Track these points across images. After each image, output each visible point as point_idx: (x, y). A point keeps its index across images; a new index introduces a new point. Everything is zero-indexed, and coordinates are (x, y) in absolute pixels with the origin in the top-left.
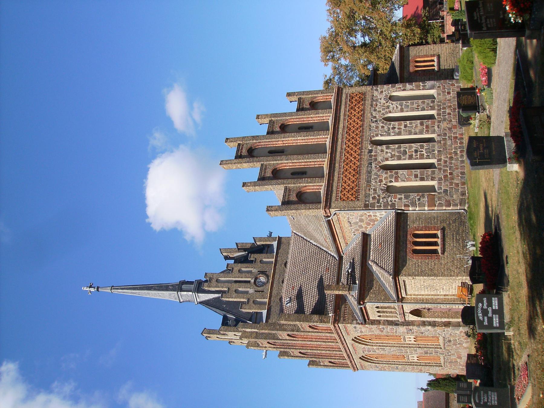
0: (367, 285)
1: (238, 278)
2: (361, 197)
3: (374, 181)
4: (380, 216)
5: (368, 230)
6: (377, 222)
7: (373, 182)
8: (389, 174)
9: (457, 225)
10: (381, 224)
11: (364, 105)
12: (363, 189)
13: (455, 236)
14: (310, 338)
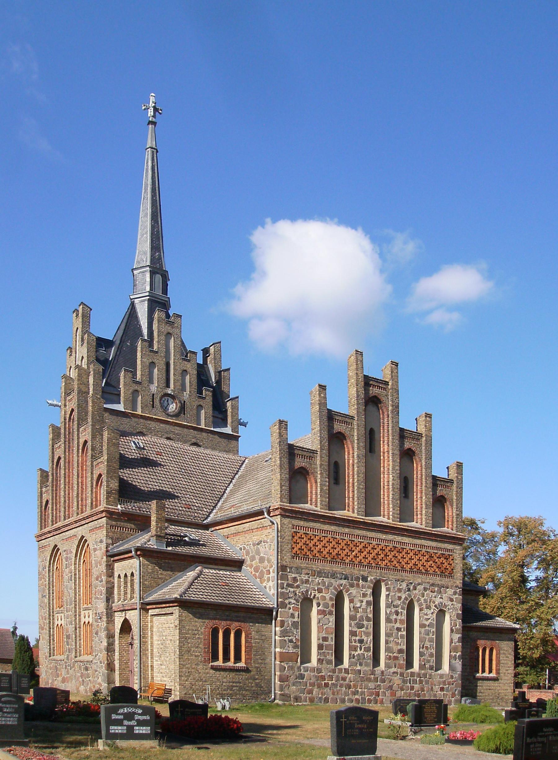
0: (165, 562)
1: (174, 369)
2: (298, 562)
3: (320, 581)
4: (268, 586)
5: (248, 568)
6: (259, 582)
9: (254, 688)
12: (310, 566)
13: (238, 684)
14: (82, 474)
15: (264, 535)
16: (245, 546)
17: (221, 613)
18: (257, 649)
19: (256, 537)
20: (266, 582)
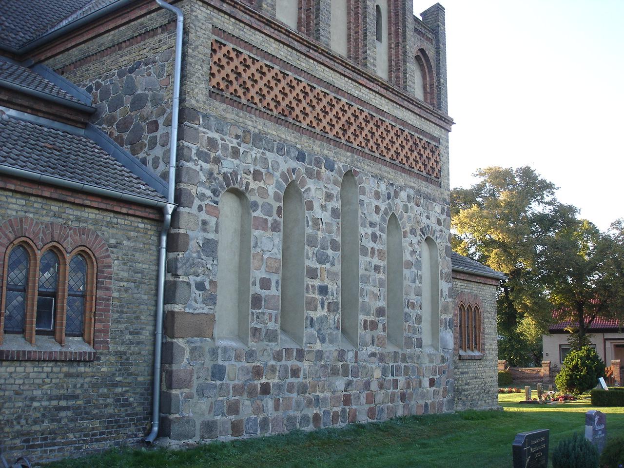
2: (219, 108)
3: (258, 155)
4: (150, 159)
5: (104, 126)
6: (128, 152)
7: (255, 152)
8: (276, 205)
9: (110, 410)
10: (120, 164)
11: (419, 176)
12: (241, 120)
13: (71, 403)
15: (148, 49)
16: (100, 81)
17: (39, 206)
18: (121, 306)
19: (126, 58)
20: (146, 149)
